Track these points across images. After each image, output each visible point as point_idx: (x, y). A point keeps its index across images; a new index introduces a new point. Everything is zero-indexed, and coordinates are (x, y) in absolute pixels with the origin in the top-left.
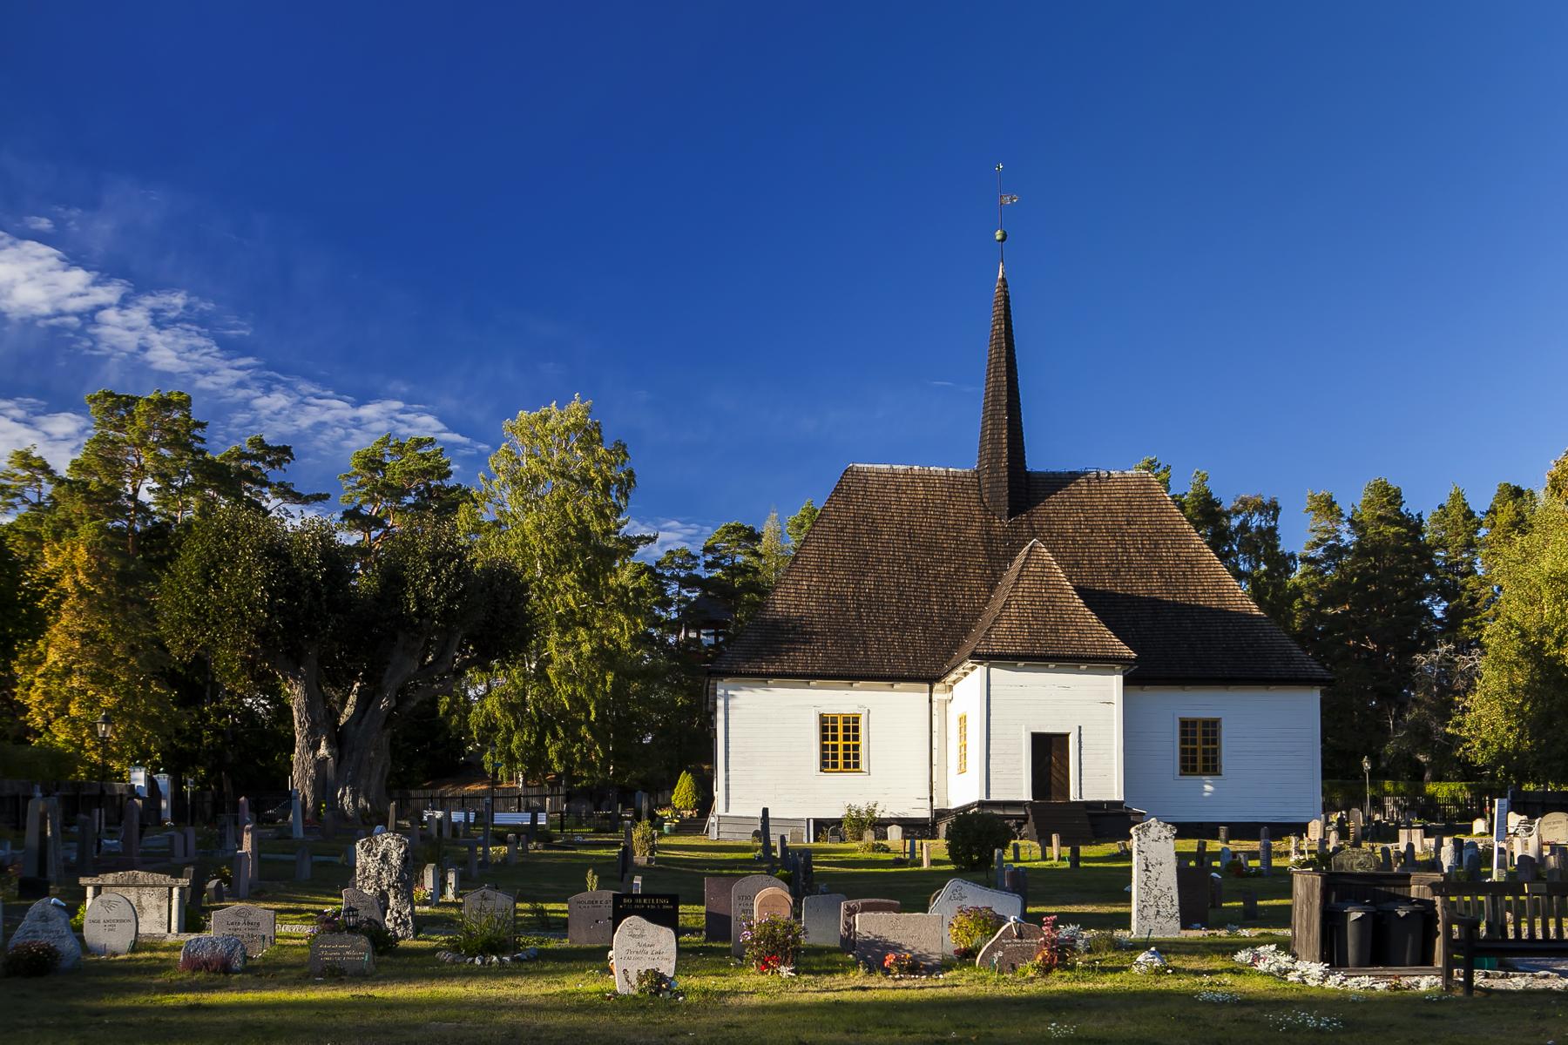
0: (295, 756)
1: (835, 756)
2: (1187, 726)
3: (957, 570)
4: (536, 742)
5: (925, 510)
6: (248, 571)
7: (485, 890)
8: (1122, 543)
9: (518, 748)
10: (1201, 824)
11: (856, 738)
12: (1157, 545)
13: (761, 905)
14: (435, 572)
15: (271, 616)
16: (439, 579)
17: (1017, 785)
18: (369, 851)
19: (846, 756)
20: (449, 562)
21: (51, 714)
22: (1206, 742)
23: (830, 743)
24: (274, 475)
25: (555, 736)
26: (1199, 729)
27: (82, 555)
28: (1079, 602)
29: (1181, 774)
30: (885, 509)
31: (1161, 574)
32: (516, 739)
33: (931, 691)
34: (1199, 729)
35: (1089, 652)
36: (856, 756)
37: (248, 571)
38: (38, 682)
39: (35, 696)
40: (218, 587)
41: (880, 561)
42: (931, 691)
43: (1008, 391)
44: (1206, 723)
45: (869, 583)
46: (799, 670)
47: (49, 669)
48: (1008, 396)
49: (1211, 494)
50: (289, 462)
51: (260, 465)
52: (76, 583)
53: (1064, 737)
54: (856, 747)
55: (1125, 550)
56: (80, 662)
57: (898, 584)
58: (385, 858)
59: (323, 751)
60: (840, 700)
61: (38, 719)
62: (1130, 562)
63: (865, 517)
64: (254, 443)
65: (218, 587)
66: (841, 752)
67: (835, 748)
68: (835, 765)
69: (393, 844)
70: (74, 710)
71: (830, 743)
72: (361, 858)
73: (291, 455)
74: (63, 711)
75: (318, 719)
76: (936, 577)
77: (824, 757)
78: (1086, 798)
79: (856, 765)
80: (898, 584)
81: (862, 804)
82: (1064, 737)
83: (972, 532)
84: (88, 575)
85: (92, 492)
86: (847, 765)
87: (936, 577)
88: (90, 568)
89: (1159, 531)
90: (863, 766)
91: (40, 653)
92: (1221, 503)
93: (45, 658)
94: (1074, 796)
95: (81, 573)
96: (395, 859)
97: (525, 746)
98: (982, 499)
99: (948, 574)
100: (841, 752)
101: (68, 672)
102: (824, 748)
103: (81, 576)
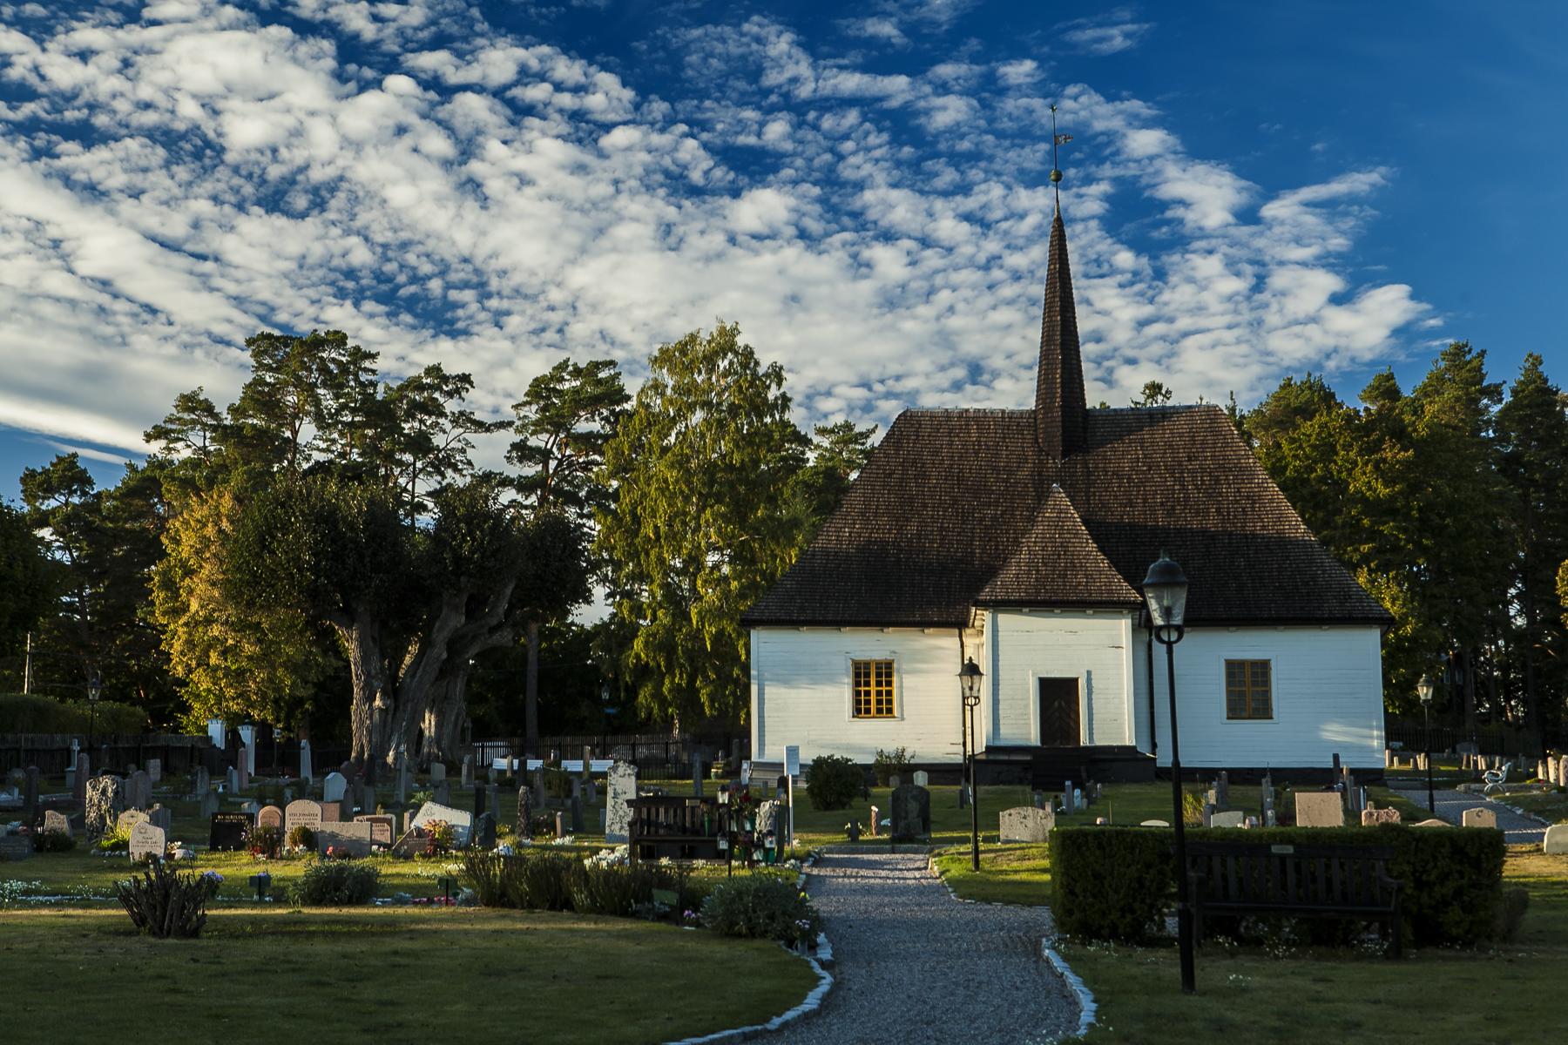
0: (353, 707)
1: (868, 702)
2: (1235, 669)
3: (1003, 513)
4: (688, 684)
5: (976, 453)
6: (298, 537)
7: (132, 811)
8: (1181, 480)
9: (670, 691)
10: (1252, 769)
11: (889, 684)
12: (1217, 481)
13: (263, 817)
14: (470, 533)
15: (318, 577)
16: (473, 539)
17: (1025, 727)
18: (94, 788)
19: (879, 702)
20: (485, 522)
21: (194, 664)
22: (1255, 684)
23: (862, 689)
24: (451, 406)
25: (706, 677)
26: (1248, 671)
27: (227, 503)
28: (1092, 546)
29: (1228, 718)
30: (936, 453)
31: (1218, 511)
32: (667, 681)
33: (961, 636)
34: (1248, 671)
35: (1095, 597)
36: (890, 702)
37: (298, 537)
38: (181, 630)
39: (177, 646)
40: (272, 552)
41: (925, 506)
42: (961, 636)
43: (1062, 330)
44: (1254, 663)
45: (912, 528)
46: (830, 618)
47: (193, 617)
48: (1062, 335)
49: (1546, 381)
50: (467, 390)
51: (437, 395)
52: (220, 531)
53: (1073, 682)
54: (889, 693)
55: (1183, 487)
56: (221, 611)
57: (942, 529)
58: (104, 792)
59: (378, 703)
60: (870, 644)
61: (179, 668)
62: (1187, 499)
63: (914, 462)
64: (430, 371)
65: (272, 552)
66: (873, 698)
67: (868, 693)
68: (868, 711)
69: (109, 782)
70: (214, 659)
71: (884, 689)
72: (89, 792)
73: (471, 383)
74: (203, 662)
75: (373, 671)
76: (981, 520)
77: (858, 702)
78: (1098, 742)
79: (890, 711)
80: (942, 529)
81: (890, 748)
82: (1073, 682)
83: (1023, 474)
84: (232, 523)
85: (246, 437)
86: (879, 711)
87: (981, 520)
88: (235, 515)
89: (1222, 467)
90: (896, 712)
91: (183, 603)
92: (1558, 390)
93: (189, 606)
94: (1084, 740)
95: (225, 520)
96: (110, 794)
97: (676, 689)
98: (1036, 439)
99: (994, 518)
100: (873, 698)
101: (209, 621)
102: (858, 693)
103: (225, 525)
